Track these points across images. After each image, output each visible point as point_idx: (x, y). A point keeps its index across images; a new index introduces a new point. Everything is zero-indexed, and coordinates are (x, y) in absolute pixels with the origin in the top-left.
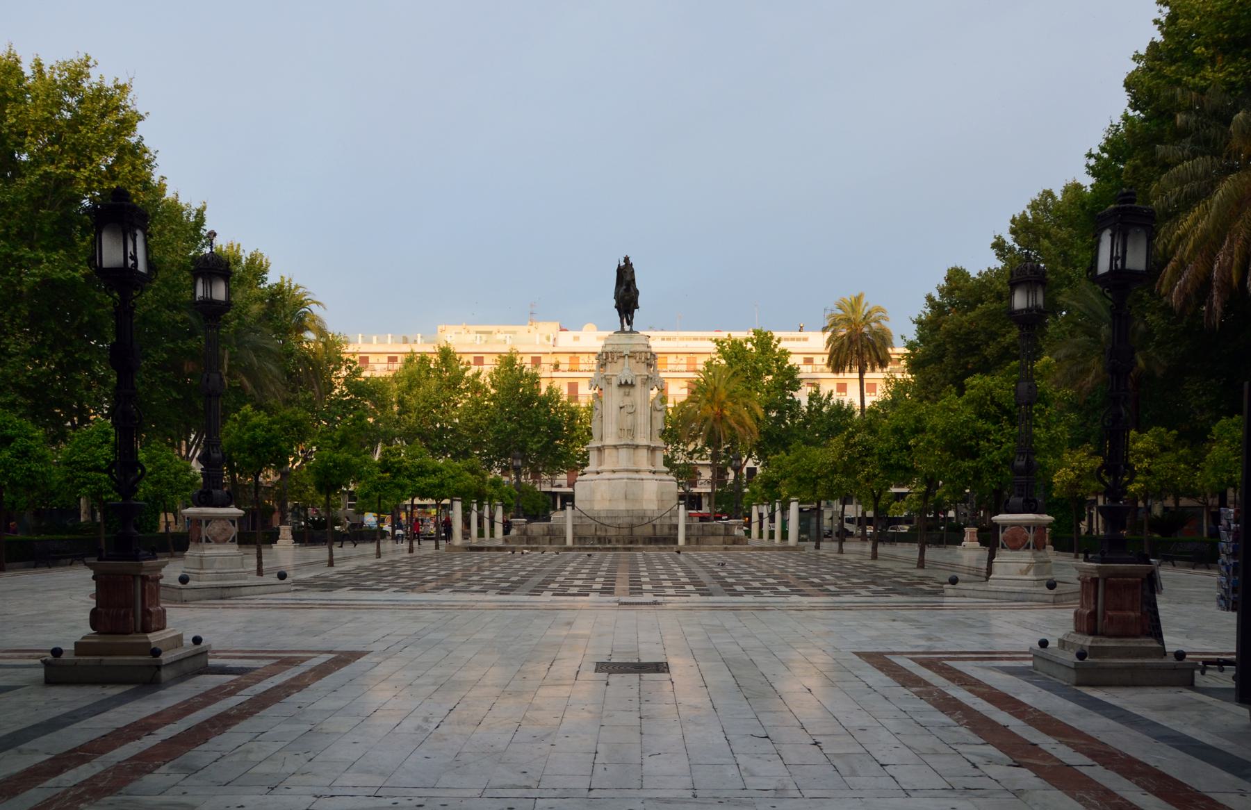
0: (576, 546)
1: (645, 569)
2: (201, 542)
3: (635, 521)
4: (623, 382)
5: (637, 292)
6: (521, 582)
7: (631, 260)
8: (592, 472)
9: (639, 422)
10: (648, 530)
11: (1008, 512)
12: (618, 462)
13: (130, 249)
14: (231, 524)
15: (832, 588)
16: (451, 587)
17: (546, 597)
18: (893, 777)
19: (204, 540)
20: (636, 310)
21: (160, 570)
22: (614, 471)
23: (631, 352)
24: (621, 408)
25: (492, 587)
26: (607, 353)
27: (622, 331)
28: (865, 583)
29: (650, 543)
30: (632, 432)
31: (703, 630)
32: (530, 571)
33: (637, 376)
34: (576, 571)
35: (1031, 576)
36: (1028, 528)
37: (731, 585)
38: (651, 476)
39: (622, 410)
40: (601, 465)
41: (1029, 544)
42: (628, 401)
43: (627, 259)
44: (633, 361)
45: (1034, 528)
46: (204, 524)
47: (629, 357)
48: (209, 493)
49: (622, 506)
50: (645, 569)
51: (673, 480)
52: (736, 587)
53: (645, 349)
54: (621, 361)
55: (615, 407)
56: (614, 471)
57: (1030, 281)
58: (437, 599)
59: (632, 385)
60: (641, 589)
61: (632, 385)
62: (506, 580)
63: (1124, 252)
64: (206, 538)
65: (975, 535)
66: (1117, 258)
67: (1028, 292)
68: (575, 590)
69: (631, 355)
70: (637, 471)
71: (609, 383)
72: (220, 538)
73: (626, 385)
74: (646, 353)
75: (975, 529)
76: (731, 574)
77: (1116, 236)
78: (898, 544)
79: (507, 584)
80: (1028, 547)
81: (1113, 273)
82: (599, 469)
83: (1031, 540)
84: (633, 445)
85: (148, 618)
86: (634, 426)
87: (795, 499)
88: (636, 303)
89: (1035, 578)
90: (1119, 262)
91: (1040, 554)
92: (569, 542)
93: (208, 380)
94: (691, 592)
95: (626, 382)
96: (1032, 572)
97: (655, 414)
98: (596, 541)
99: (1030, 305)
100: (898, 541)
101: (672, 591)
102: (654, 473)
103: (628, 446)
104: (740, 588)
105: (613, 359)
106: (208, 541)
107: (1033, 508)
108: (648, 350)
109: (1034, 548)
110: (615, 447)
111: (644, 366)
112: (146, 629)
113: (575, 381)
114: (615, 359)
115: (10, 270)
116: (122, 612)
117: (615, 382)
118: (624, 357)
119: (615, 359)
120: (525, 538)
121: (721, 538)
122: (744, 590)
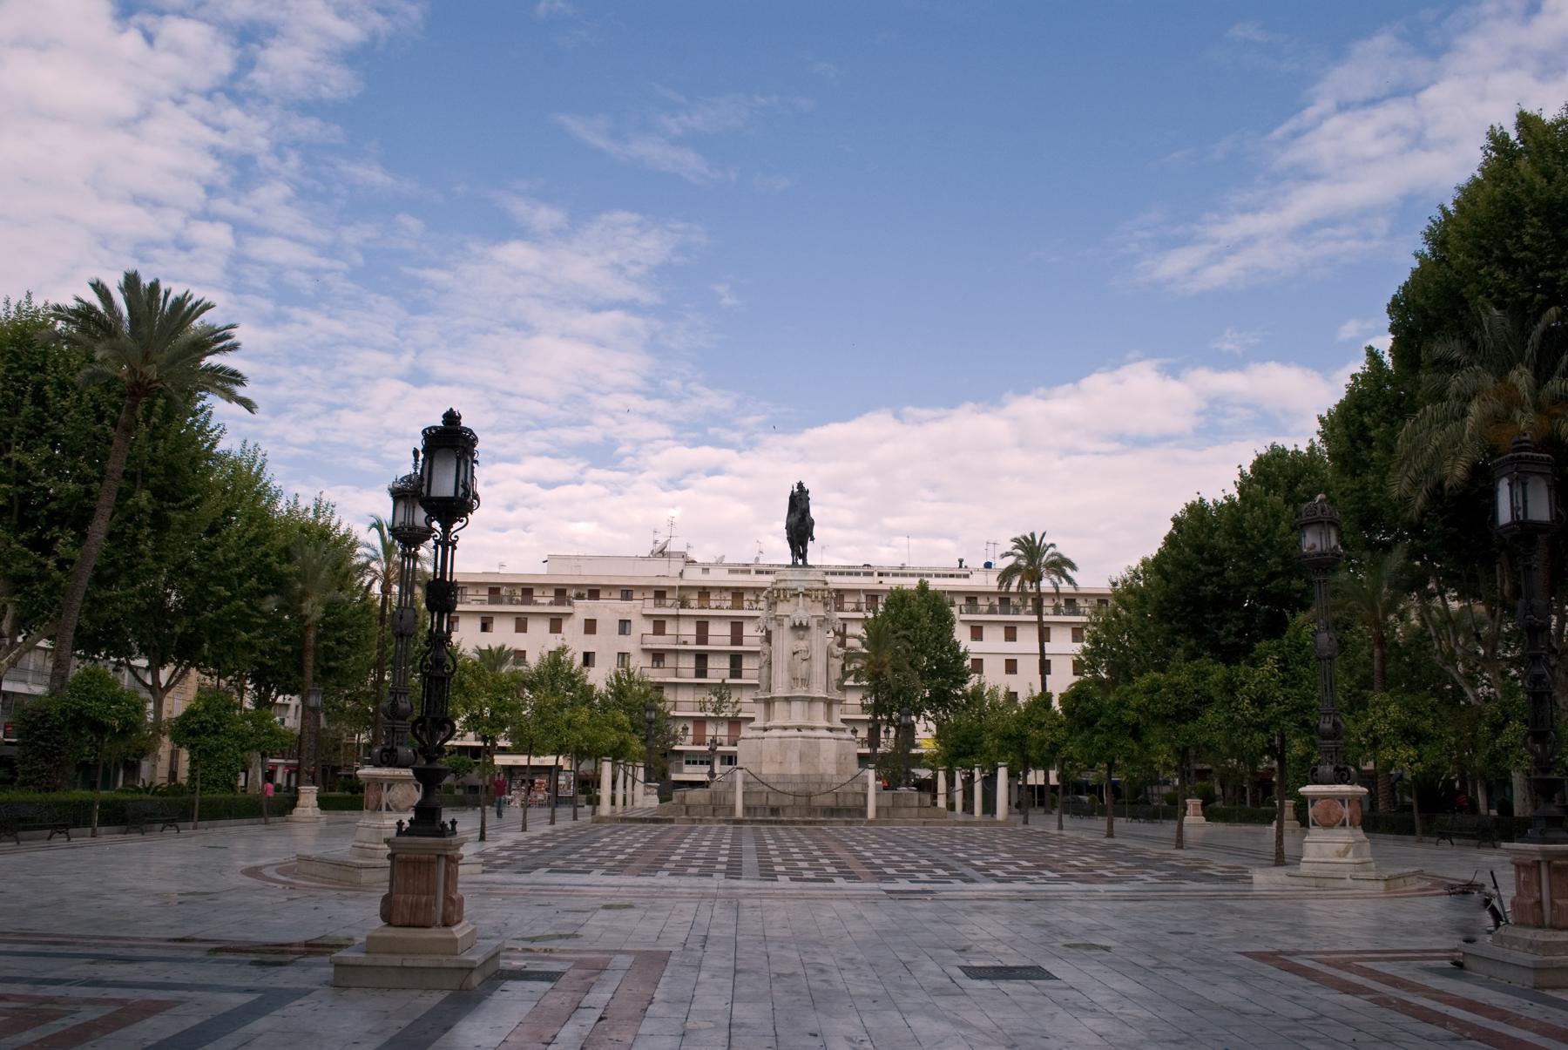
0: (747, 818)
2: (380, 809)
3: (812, 788)
4: (797, 624)
6: (631, 859)
7: (806, 486)
9: (814, 670)
10: (828, 801)
11: (1316, 783)
13: (462, 477)
14: (415, 788)
15: (999, 873)
16: (547, 865)
17: (663, 879)
19: (384, 807)
21: (458, 849)
22: (785, 728)
24: (794, 654)
25: (598, 865)
26: (779, 590)
27: (795, 564)
28: (1038, 867)
29: (832, 815)
30: (806, 682)
32: (638, 848)
34: (715, 847)
35: (1350, 858)
36: (1342, 801)
37: (880, 867)
38: (828, 734)
40: (769, 720)
41: (1345, 821)
42: (802, 645)
43: (800, 485)
44: (808, 599)
46: (385, 787)
47: (804, 595)
48: (393, 751)
49: (795, 769)
52: (835, 871)
53: (821, 586)
54: (793, 600)
55: (787, 652)
56: (785, 728)
57: (1323, 522)
58: (573, 882)
60: (773, 870)
61: (807, 628)
62: (611, 858)
63: (1525, 502)
64: (387, 805)
65: (1200, 807)
66: (1519, 509)
67: (1321, 533)
68: (695, 870)
70: (813, 729)
71: (780, 625)
72: (402, 806)
73: (800, 628)
74: (823, 590)
75: (1199, 801)
76: (877, 856)
77: (1515, 485)
78: (1099, 818)
80: (1344, 825)
81: (1515, 521)
82: (768, 725)
84: (808, 697)
85: (451, 908)
86: (809, 674)
88: (811, 534)
89: (1356, 861)
90: (1520, 513)
92: (739, 813)
93: (401, 618)
94: (834, 875)
95: (801, 624)
96: (1351, 854)
97: (833, 661)
98: (768, 812)
99: (1324, 548)
100: (1099, 815)
103: (803, 699)
104: (890, 871)
105: (785, 596)
106: (388, 809)
107: (1345, 777)
108: (826, 587)
110: (787, 700)
111: (821, 605)
112: (447, 924)
113: (663, 619)
115: (1556, 326)
116: (424, 899)
117: (787, 623)
118: (798, 595)
120: (683, 807)
121: (915, 811)
122: (896, 872)
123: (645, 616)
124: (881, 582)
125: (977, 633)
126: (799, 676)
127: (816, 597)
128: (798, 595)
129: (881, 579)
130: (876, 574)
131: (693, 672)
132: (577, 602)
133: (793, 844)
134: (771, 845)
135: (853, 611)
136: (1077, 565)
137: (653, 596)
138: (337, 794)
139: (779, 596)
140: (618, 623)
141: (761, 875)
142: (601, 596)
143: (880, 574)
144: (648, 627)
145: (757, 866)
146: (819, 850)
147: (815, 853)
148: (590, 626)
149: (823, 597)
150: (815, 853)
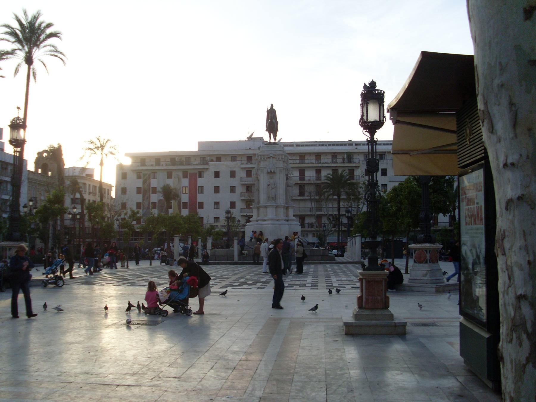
1: (333, 275)
4: (269, 171)
5: (277, 123)
8: (254, 221)
12: (267, 215)
18: (102, 154)
20: (277, 132)
23: (273, 155)
30: (274, 198)
31: (513, 315)
33: (277, 168)
39: (269, 186)
45: (430, 251)
46: (8, 250)
50: (333, 275)
51: (298, 225)
59: (274, 173)
61: (274, 173)
69: (274, 156)
74: (282, 155)
79: (261, 284)
80: (426, 262)
83: (428, 258)
87: (359, 235)
89: (430, 279)
91: (433, 265)
95: (271, 171)
96: (428, 276)
101: (349, 287)
102: (288, 221)
109: (430, 262)
110: (266, 207)
114: (265, 159)
119: (265, 159)
123: (242, 168)
124: (357, 148)
125: (290, 175)
126: (270, 196)
127: (279, 158)
128: (269, 158)
129: (356, 147)
130: (354, 144)
131: (298, 194)
132: (210, 163)
133: (342, 274)
134: (338, 270)
135: (341, 163)
136: (14, 17)
137: (246, 159)
138: (315, 248)
139: (261, 159)
140: (420, 52)
141: (326, 284)
142: (222, 160)
143: (356, 145)
144: (244, 174)
145: (319, 282)
146: (353, 276)
147: (352, 277)
148: (217, 174)
149: (282, 158)
150: (352, 277)
